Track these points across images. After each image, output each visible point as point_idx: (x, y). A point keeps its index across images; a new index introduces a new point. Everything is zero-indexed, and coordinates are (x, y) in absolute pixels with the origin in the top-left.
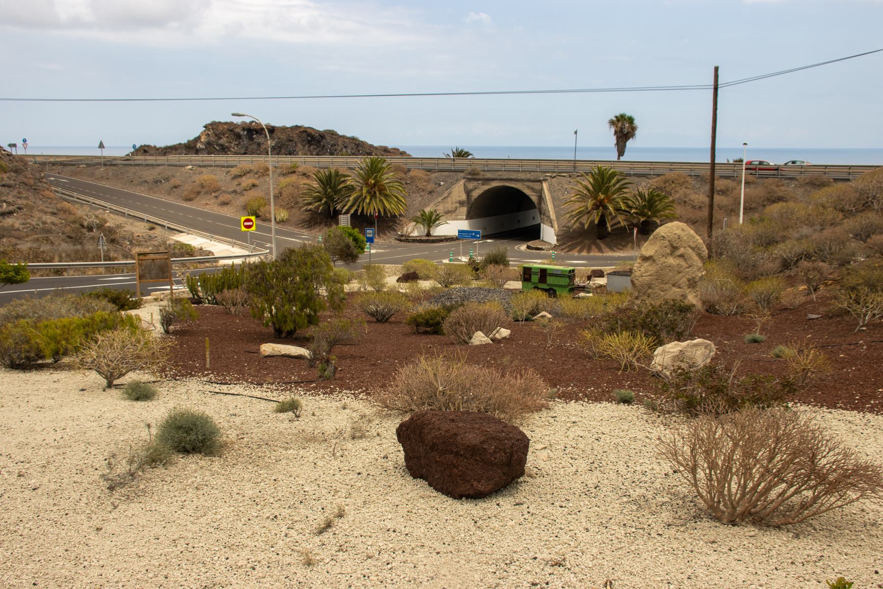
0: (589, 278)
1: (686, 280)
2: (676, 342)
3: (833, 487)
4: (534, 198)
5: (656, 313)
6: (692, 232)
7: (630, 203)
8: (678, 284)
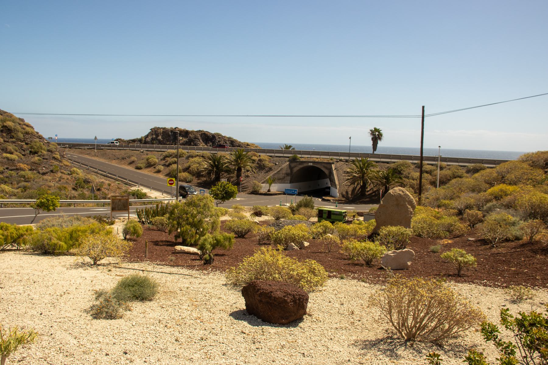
3: (458, 323)
4: (327, 172)
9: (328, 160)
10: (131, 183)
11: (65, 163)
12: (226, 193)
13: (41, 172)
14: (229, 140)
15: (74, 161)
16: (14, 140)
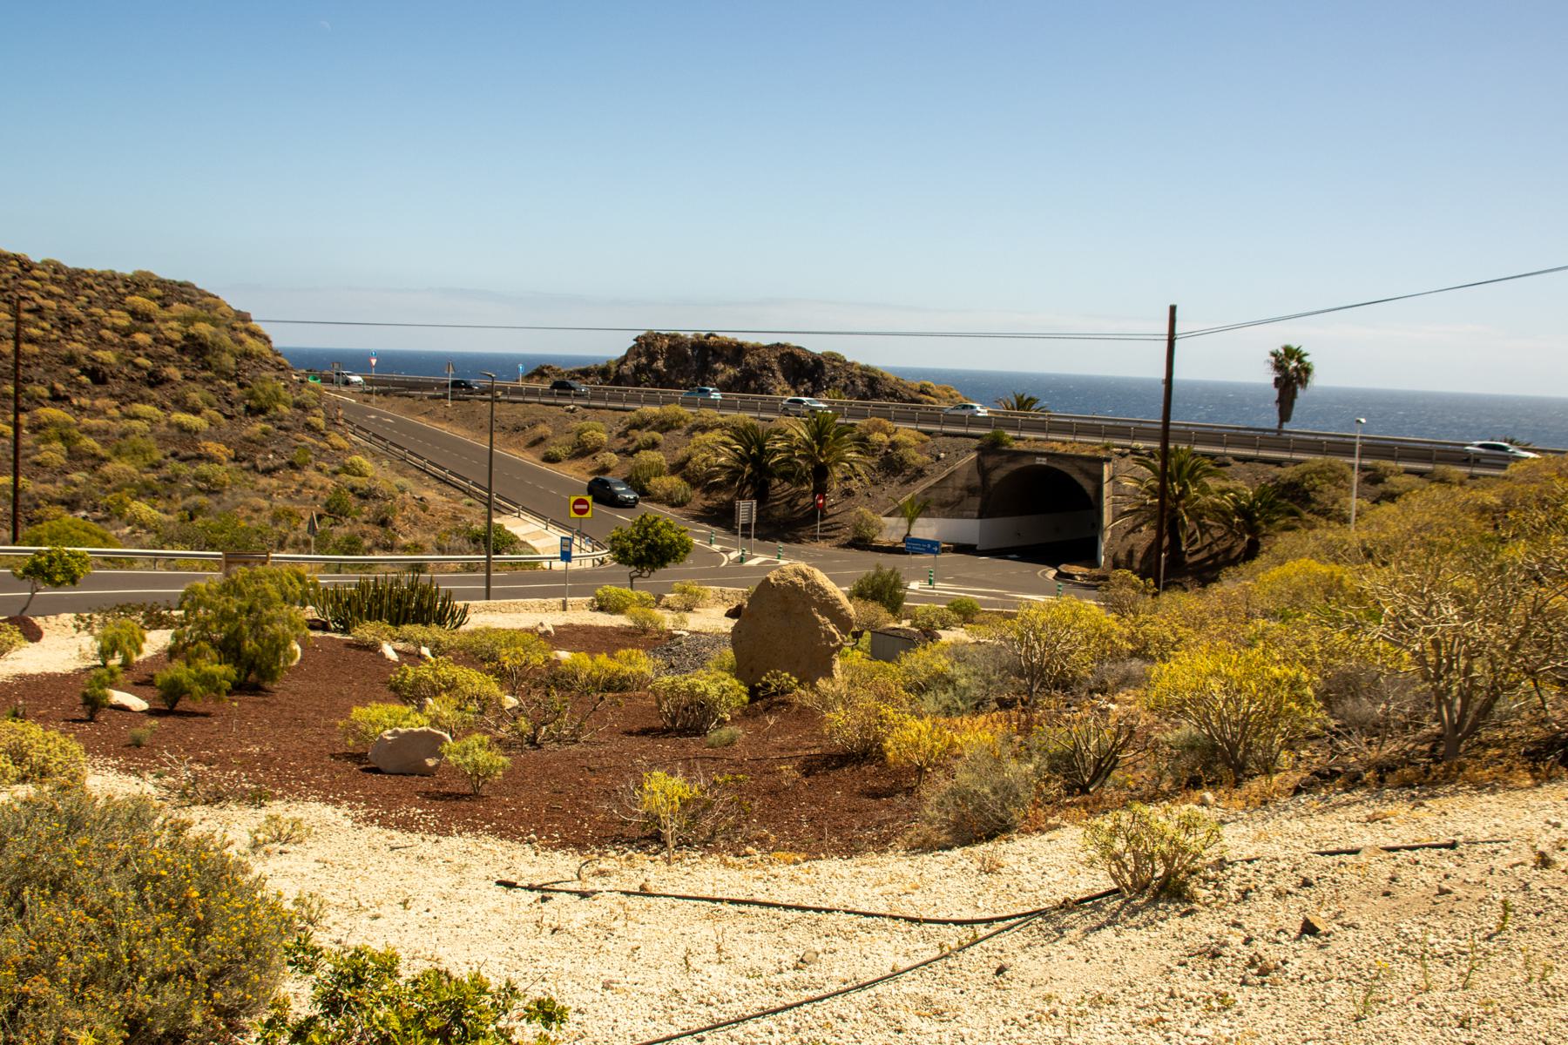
4: (1088, 486)
9: (1095, 451)
10: (503, 503)
11: (334, 441)
12: (650, 548)
13: (261, 465)
14: (862, 376)
15: (374, 435)
16: (209, 374)
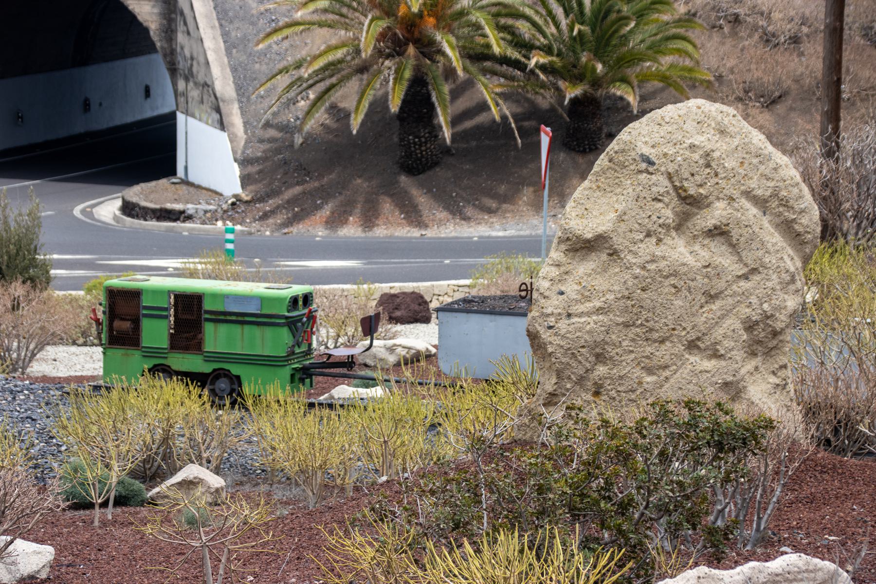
0: (369, 326)
1: (738, 325)
2: (703, 569)
5: (624, 457)
6: (758, 138)
7: (523, 27)
8: (707, 341)
